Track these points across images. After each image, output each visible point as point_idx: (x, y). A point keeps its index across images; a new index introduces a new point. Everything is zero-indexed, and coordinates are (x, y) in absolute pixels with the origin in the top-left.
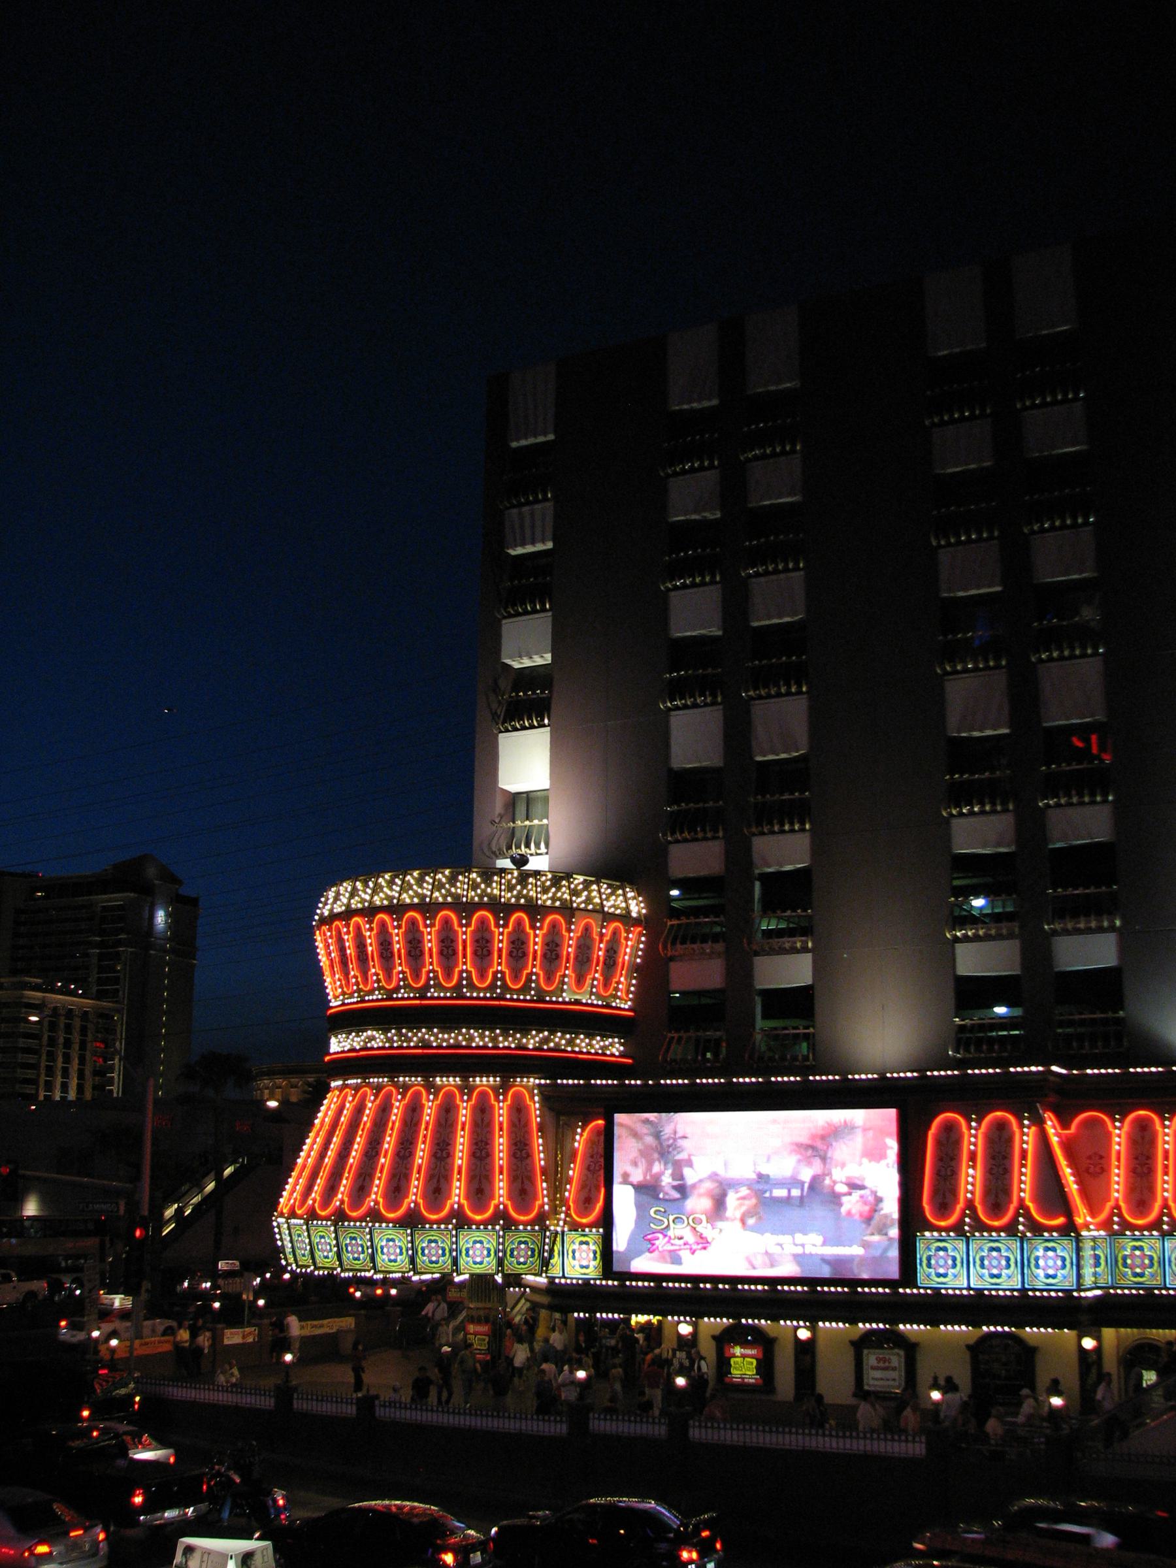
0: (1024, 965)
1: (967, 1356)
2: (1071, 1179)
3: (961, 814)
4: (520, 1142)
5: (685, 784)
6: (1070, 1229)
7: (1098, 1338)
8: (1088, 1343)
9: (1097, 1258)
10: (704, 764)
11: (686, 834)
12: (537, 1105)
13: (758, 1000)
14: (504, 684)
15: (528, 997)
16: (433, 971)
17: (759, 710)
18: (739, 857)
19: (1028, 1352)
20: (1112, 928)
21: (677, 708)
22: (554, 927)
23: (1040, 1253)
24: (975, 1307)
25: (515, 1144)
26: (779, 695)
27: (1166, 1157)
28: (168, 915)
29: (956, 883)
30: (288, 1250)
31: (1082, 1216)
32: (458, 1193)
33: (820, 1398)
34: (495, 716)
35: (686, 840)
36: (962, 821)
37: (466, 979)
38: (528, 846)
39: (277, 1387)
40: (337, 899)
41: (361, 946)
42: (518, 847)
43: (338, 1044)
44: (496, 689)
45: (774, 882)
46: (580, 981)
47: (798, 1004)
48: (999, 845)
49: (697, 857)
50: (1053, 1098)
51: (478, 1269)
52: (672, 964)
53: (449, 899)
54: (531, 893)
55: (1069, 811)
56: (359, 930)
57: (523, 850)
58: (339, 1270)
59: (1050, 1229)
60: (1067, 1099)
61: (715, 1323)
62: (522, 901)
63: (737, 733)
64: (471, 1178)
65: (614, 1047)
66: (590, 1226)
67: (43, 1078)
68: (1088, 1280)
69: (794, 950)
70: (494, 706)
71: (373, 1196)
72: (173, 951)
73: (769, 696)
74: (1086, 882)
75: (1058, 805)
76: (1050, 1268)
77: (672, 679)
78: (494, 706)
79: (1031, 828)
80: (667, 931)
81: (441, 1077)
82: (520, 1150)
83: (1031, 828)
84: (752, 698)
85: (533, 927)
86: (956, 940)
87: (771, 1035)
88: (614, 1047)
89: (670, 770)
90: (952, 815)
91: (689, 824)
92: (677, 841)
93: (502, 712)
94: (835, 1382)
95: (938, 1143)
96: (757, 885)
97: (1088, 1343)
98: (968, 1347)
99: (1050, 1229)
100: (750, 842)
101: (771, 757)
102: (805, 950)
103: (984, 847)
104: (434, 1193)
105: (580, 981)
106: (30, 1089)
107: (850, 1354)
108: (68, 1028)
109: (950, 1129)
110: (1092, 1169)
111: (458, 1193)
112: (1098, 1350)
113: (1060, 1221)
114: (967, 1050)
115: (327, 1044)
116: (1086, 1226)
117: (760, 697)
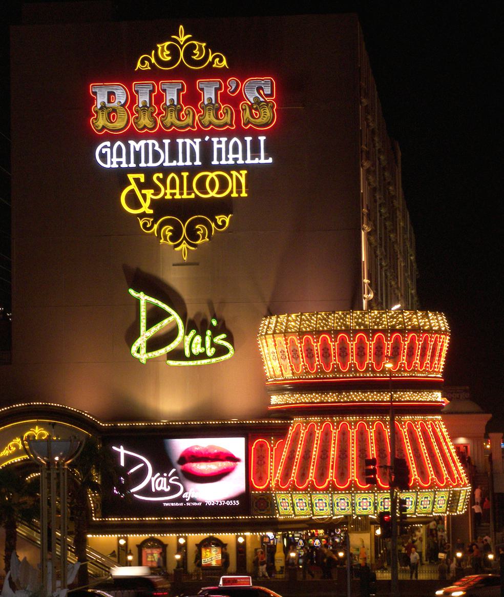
4: (363, 449)
12: (389, 430)
15: (351, 375)
16: (336, 364)
22: (379, 339)
25: (360, 451)
27: (281, 465)
30: (66, 518)
32: (331, 474)
37: (353, 367)
41: (423, 355)
53: (343, 328)
54: (366, 323)
58: (293, 515)
62: (362, 327)
64: (338, 468)
71: (292, 479)
81: (349, 417)
104: (302, 476)
109: (262, 445)
111: (331, 474)
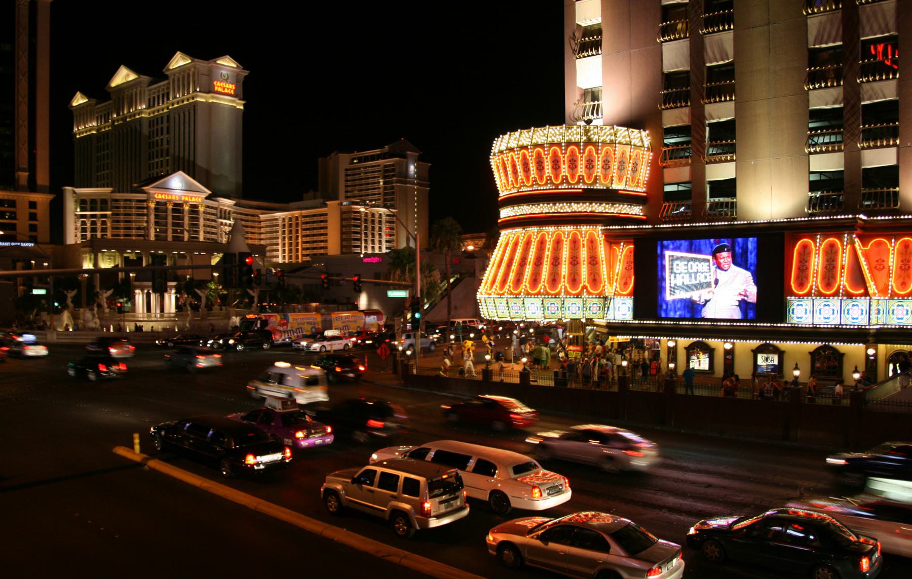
0: (845, 166)
1: (809, 357)
2: (867, 271)
3: (814, 88)
5: (670, 79)
6: (866, 294)
7: (876, 349)
8: (871, 352)
9: (878, 310)
10: (681, 69)
11: (671, 105)
13: (708, 187)
14: (578, 34)
17: (708, 40)
18: (698, 116)
19: (839, 356)
20: (895, 145)
21: (666, 41)
23: (850, 307)
24: (811, 333)
26: (719, 31)
28: (415, 167)
29: (811, 125)
31: (872, 288)
33: (737, 376)
34: (574, 51)
35: (671, 108)
36: (815, 92)
38: (592, 114)
39: (483, 370)
40: (501, 143)
42: (588, 115)
43: (506, 213)
44: (574, 37)
45: (717, 128)
46: (620, 179)
47: (727, 188)
48: (834, 103)
49: (675, 117)
50: (859, 231)
51: (574, 317)
52: (665, 170)
55: (875, 85)
56: (513, 156)
57: (591, 117)
59: (857, 296)
60: (867, 232)
61: (684, 342)
63: (697, 52)
65: (636, 211)
66: (627, 295)
67: (363, 245)
68: (873, 321)
69: (726, 161)
70: (573, 46)
72: (418, 184)
73: (714, 32)
74: (883, 123)
75: (868, 81)
76: (855, 314)
77: (663, 27)
78: (573, 46)
79: (852, 95)
80: (663, 157)
82: (593, 261)
83: (852, 95)
84: (705, 34)
85: (597, 153)
86: (810, 153)
87: (714, 206)
88: (636, 211)
89: (663, 73)
90: (809, 89)
91: (672, 100)
92: (667, 109)
93: (577, 48)
94: (743, 369)
95: (799, 254)
96: (708, 129)
97: (871, 352)
98: (810, 353)
99: (857, 296)
100: (704, 107)
101: (715, 64)
102: (732, 160)
103: (826, 105)
105: (620, 179)
106: (358, 250)
107: (752, 354)
108: (373, 222)
109: (805, 247)
110: (879, 266)
112: (875, 355)
113: (862, 291)
114: (814, 208)
115: (499, 213)
116: (875, 294)
117: (709, 33)
